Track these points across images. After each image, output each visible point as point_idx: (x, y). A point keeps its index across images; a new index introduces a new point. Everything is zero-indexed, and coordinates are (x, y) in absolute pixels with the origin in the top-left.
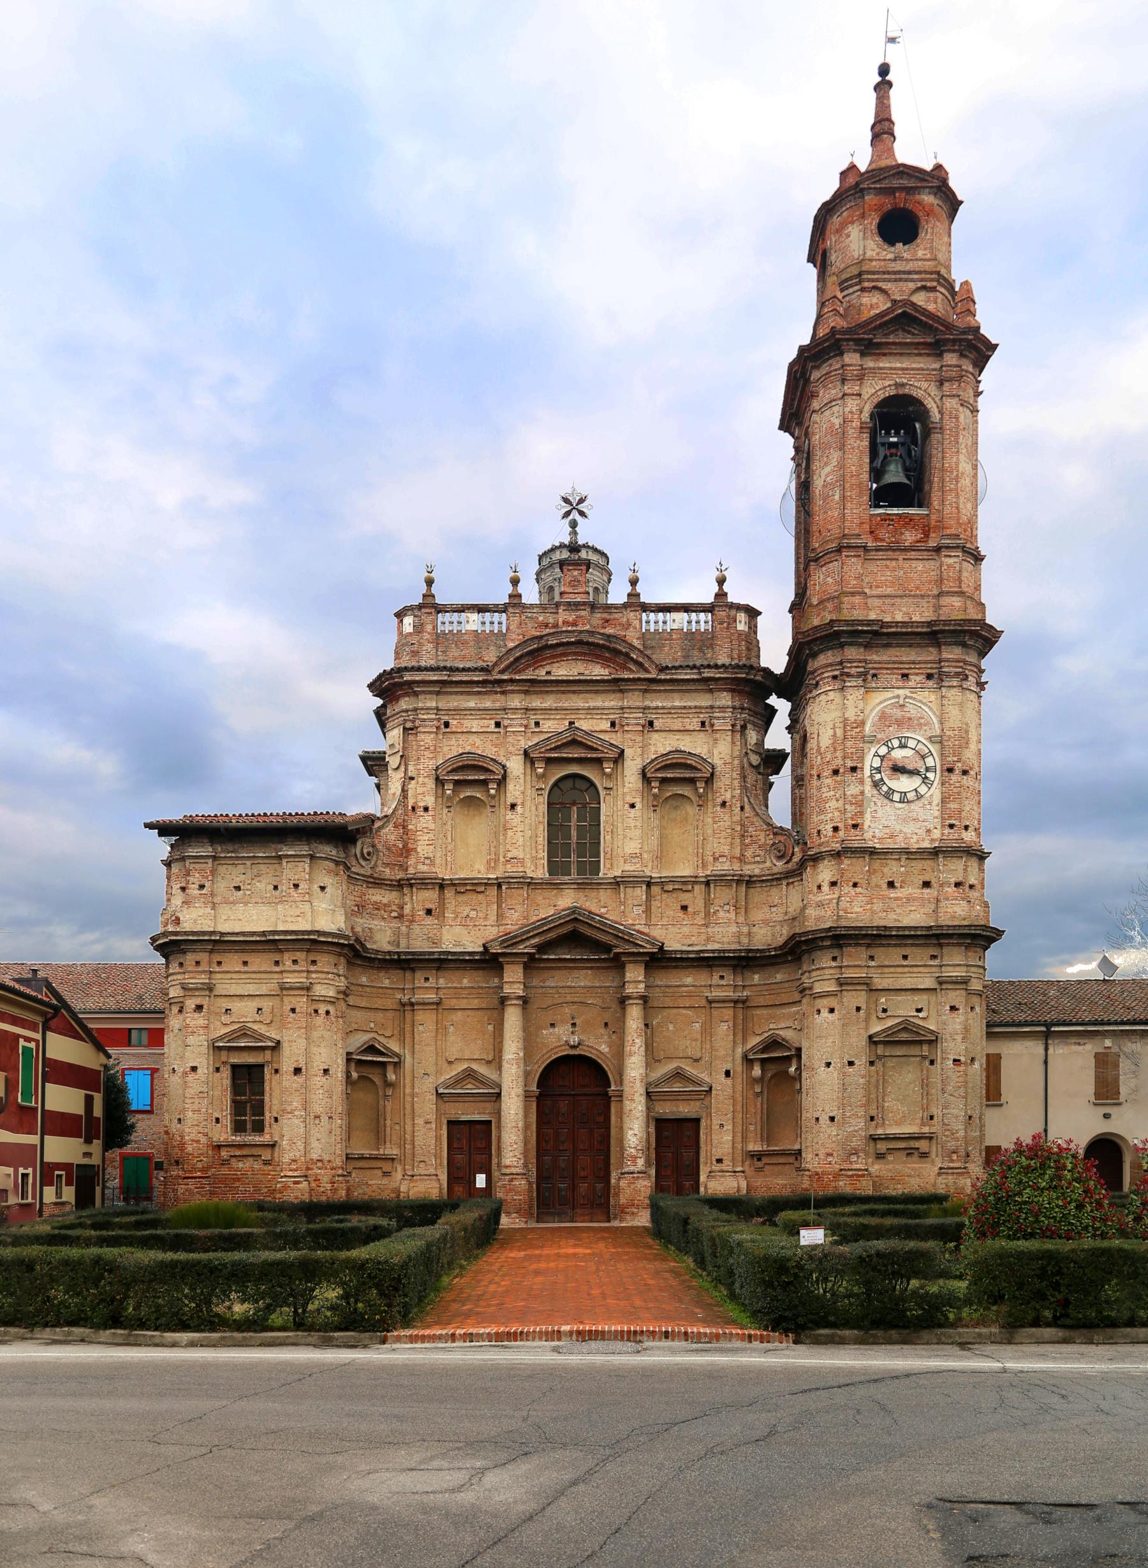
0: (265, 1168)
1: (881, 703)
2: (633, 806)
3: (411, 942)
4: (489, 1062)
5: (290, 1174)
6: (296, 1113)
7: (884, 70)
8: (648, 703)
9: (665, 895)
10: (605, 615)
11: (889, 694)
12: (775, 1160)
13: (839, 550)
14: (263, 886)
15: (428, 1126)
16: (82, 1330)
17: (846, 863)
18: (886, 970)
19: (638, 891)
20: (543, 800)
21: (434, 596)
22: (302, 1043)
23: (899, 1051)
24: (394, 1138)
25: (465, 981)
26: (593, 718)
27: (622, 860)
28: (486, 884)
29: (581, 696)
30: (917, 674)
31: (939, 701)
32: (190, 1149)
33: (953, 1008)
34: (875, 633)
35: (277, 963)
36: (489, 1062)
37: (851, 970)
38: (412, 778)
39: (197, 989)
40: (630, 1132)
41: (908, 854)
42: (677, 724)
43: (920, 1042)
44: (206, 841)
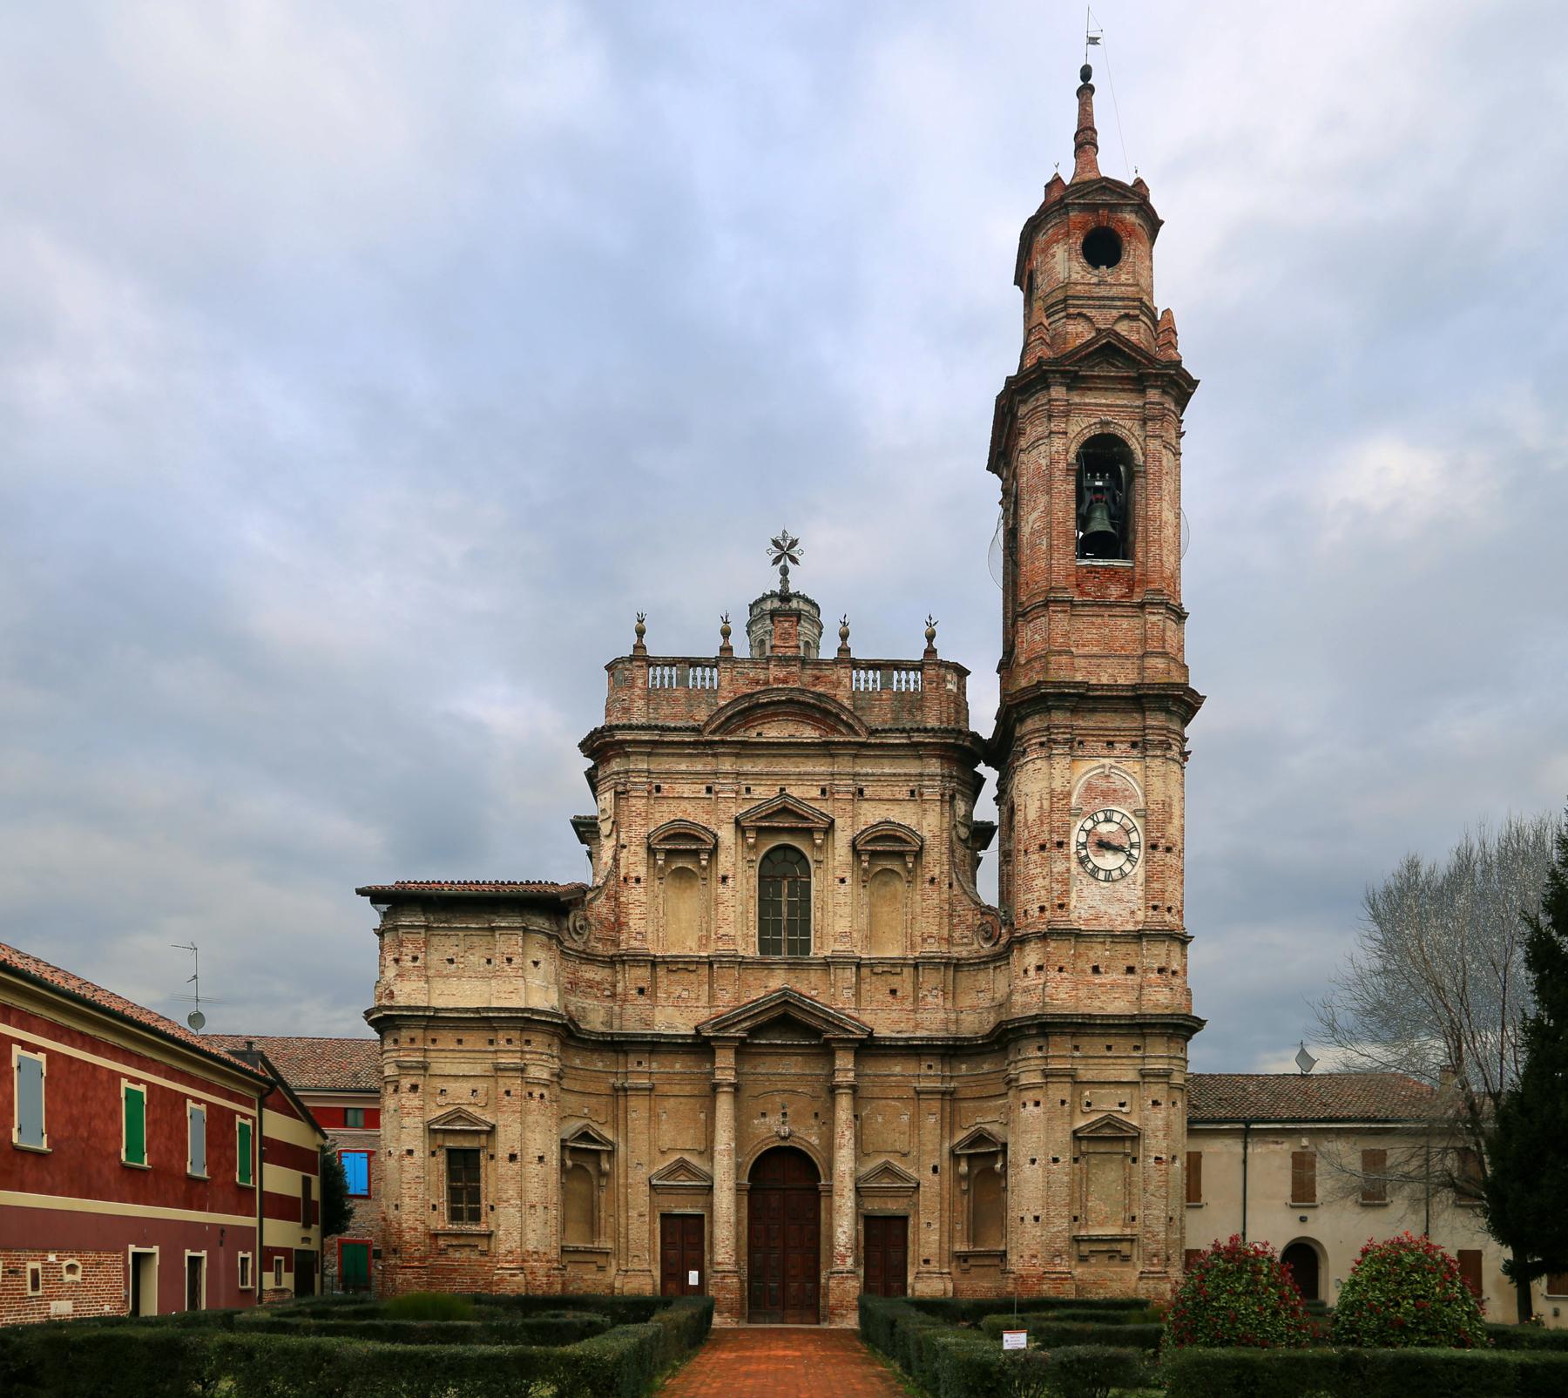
2: (842, 881)
4: (701, 1153)
7: (1086, 73)
10: (816, 672)
11: (1095, 764)
13: (1046, 605)
14: (476, 959)
18: (1091, 1061)
19: (848, 972)
22: (517, 1127)
25: (678, 1066)
32: (407, 1237)
36: (701, 1153)
38: (624, 847)
39: (411, 1068)
41: (1114, 937)
42: (886, 794)
43: (1123, 1139)
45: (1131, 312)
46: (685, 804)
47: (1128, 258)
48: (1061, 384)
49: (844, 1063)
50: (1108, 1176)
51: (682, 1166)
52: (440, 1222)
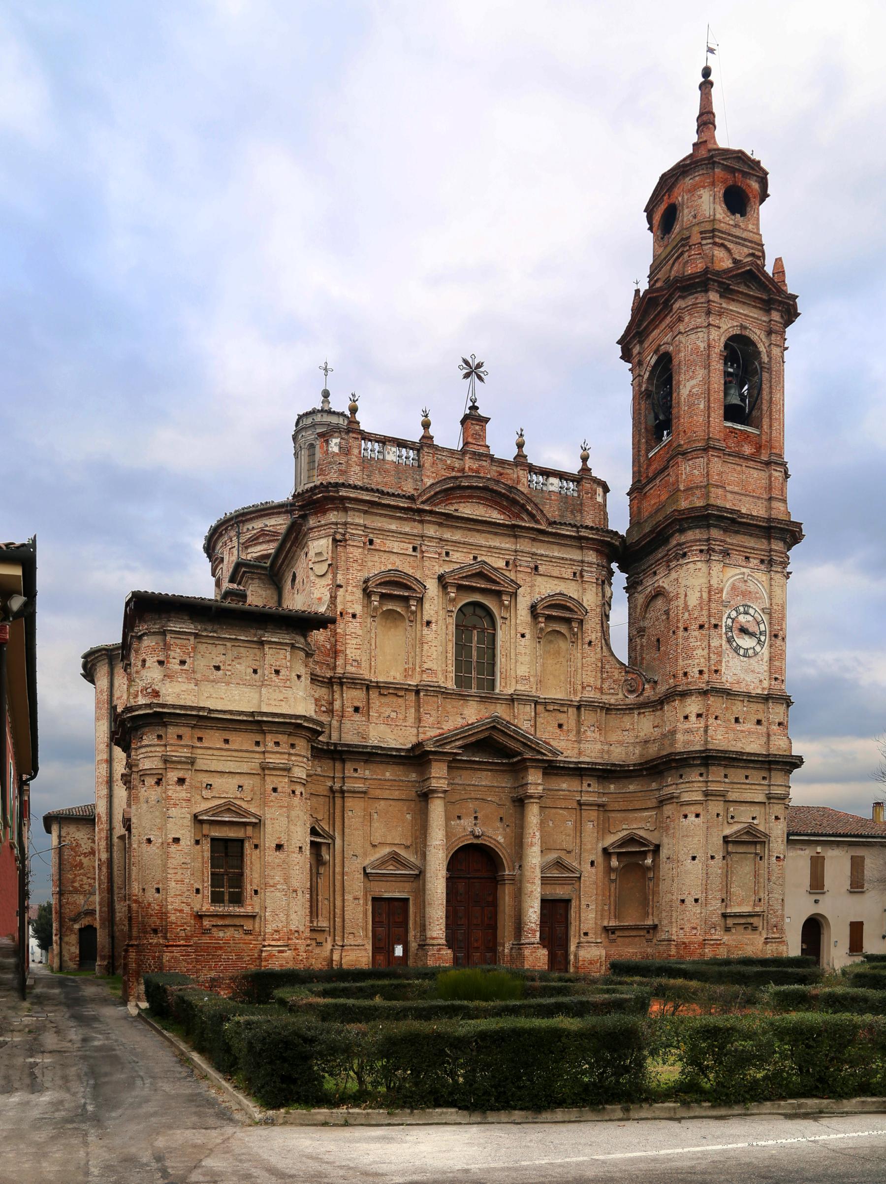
0: (246, 937)
1: (732, 576)
2: (523, 636)
3: (343, 735)
4: (407, 847)
5: (273, 943)
6: (278, 887)
7: (707, 72)
8: (534, 550)
9: (547, 714)
10: (499, 469)
11: (737, 571)
12: (626, 933)
13: (706, 449)
14: (243, 668)
15: (357, 901)
16: (817, 1101)
17: (712, 700)
18: (735, 786)
19: (528, 708)
20: (452, 621)
21: (358, 423)
22: (284, 820)
23: (741, 849)
24: (324, 912)
25: (388, 774)
26: (495, 553)
27: (514, 681)
28: (406, 690)
29: (483, 535)
30: (754, 558)
31: (768, 582)
32: (173, 918)
33: (777, 818)
34: (733, 521)
35: (258, 743)
36: (407, 847)
37: (714, 784)
38: (340, 586)
39: (179, 762)
40: (531, 910)
41: (750, 697)
42: (556, 572)
43: (755, 843)
44: (186, 618)
45: (757, 253)
46: (393, 558)
47: (750, 212)
48: (717, 291)
49: (535, 779)
50: (744, 869)
51: (394, 858)
52: (207, 907)
